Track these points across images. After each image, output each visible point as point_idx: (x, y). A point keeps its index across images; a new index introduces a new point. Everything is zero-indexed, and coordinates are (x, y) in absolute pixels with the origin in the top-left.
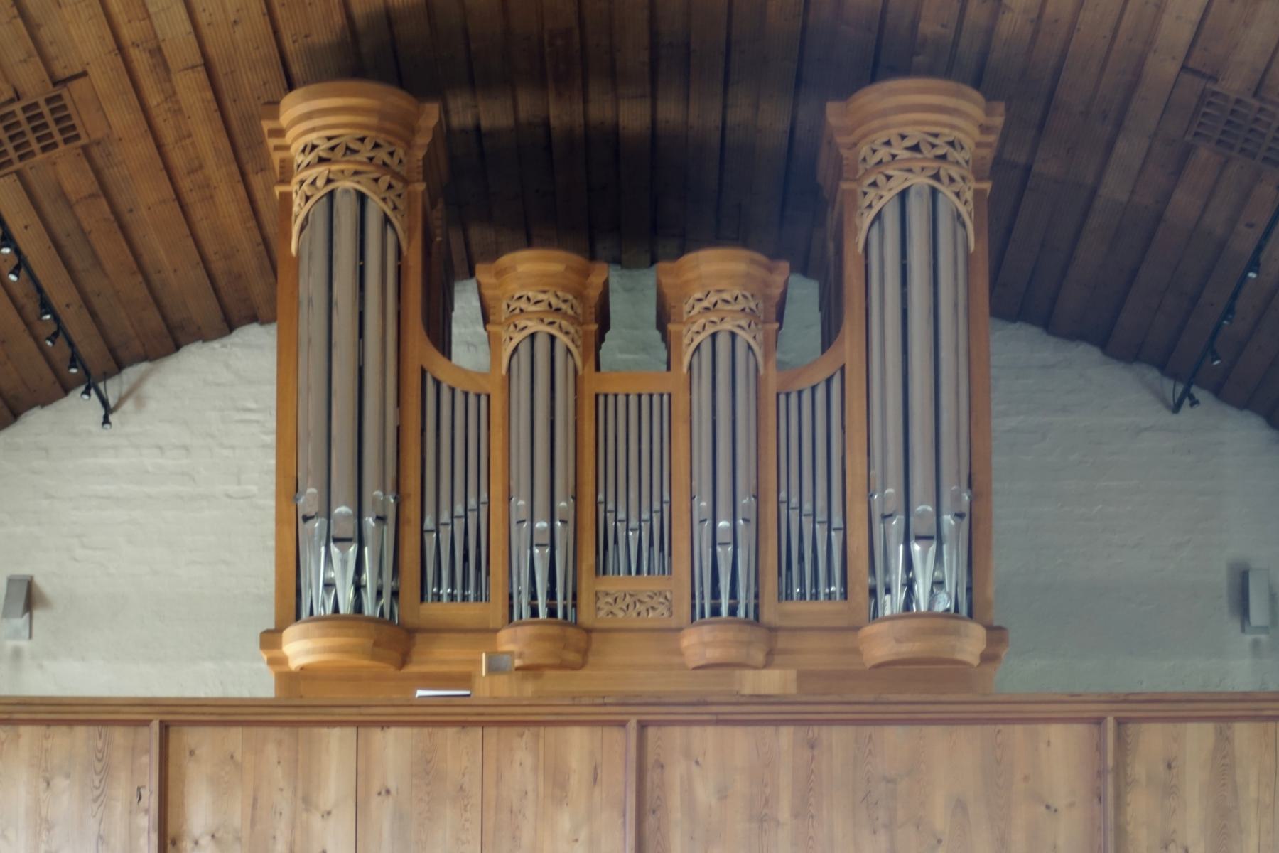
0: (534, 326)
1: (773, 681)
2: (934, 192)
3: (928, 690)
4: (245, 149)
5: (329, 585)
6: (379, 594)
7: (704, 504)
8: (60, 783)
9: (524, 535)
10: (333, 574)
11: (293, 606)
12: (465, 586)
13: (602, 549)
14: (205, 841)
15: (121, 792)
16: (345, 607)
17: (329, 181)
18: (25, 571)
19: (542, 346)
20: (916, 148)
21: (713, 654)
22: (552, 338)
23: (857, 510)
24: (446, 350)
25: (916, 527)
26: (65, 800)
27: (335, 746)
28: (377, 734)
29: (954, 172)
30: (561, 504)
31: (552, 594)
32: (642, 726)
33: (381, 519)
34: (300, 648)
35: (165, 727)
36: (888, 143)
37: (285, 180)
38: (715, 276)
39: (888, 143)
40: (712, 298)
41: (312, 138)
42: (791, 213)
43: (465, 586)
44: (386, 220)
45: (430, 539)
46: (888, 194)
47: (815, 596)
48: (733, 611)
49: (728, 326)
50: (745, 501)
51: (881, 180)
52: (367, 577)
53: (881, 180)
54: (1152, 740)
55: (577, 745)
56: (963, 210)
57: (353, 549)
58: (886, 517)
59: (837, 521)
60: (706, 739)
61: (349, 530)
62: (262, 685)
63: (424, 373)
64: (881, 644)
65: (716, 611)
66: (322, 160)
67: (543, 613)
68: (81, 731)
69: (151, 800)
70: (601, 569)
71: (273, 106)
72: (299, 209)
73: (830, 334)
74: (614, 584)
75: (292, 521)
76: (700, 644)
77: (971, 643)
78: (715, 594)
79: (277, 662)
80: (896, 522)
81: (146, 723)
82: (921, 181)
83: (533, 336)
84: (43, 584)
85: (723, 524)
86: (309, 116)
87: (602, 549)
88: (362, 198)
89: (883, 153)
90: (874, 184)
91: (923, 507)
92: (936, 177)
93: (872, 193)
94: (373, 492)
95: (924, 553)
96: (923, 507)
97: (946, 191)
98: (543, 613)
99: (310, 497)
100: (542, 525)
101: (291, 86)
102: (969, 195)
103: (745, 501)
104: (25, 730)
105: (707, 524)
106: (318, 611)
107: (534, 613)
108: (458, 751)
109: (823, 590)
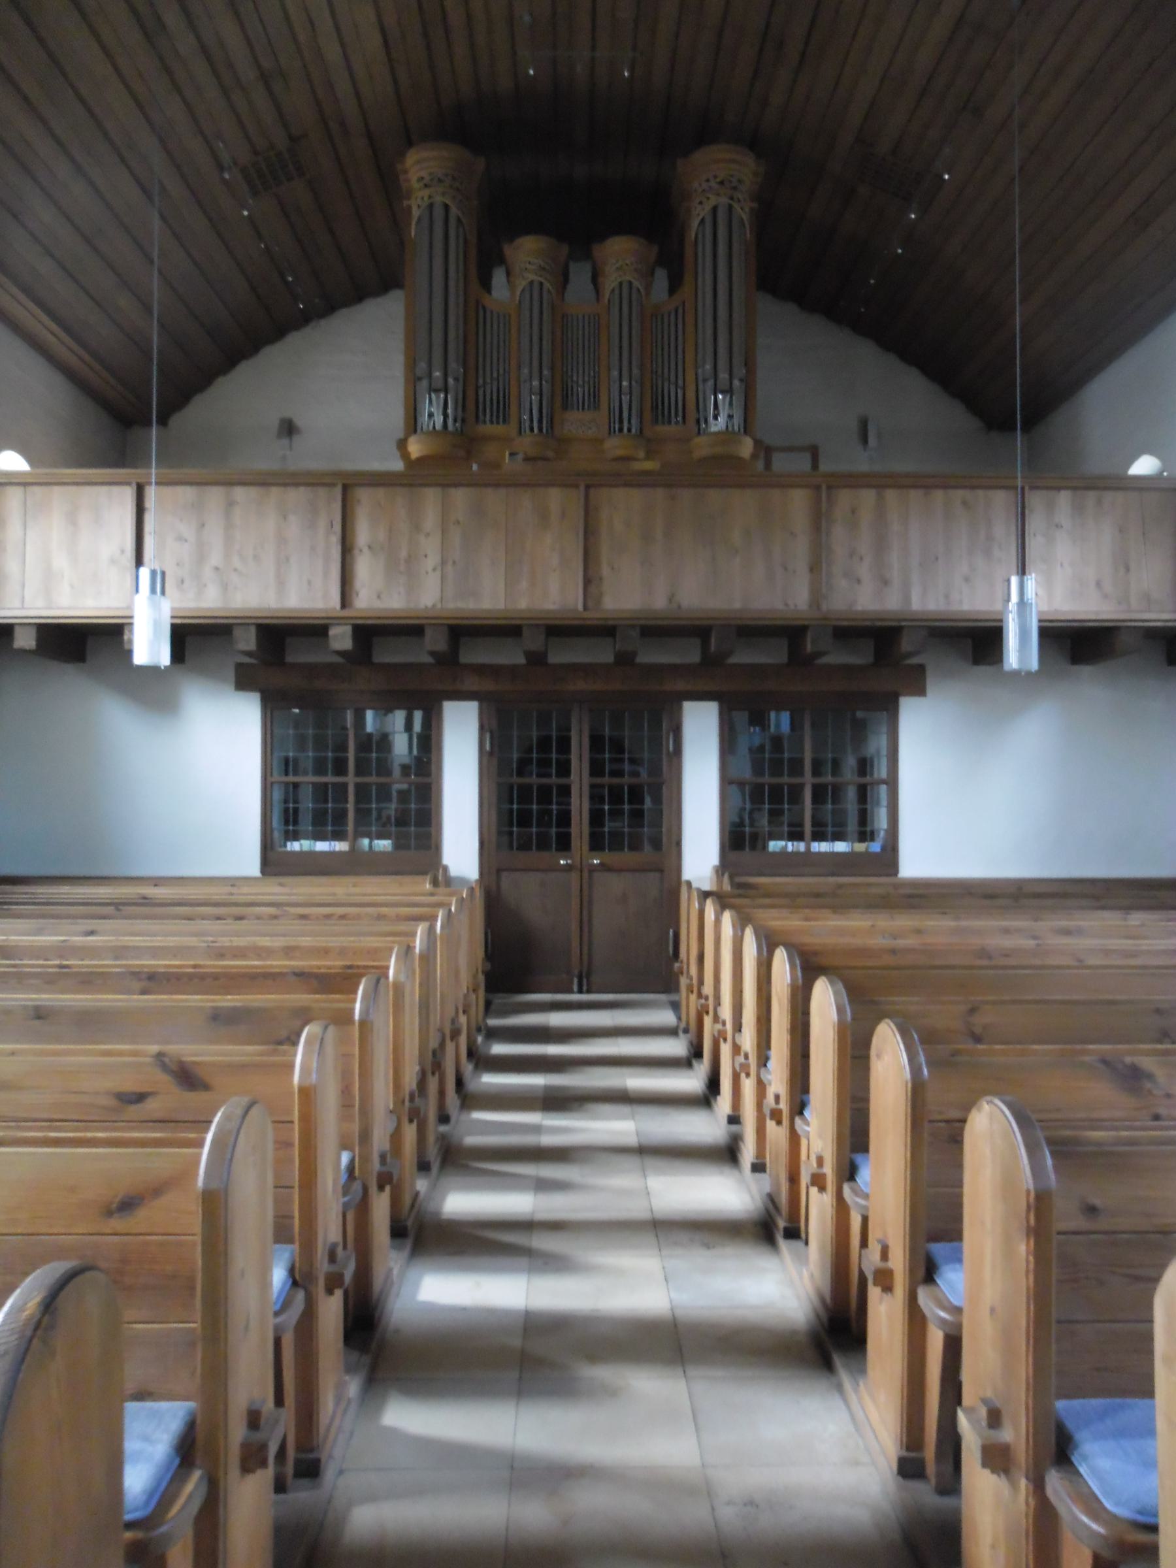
0: (531, 277)
1: (649, 465)
2: (730, 207)
3: (722, 471)
4: (391, 186)
5: (431, 415)
6: (455, 421)
7: (615, 373)
8: (292, 518)
9: (528, 396)
10: (433, 412)
11: (412, 424)
12: (498, 417)
13: (565, 398)
14: (366, 550)
15: (322, 523)
16: (439, 426)
17: (430, 197)
18: (287, 414)
19: (536, 287)
20: (722, 183)
21: (620, 452)
22: (541, 284)
23: (690, 377)
24: (489, 291)
25: (720, 386)
26: (294, 527)
27: (431, 497)
28: (453, 491)
29: (740, 197)
30: (545, 372)
31: (540, 421)
32: (588, 487)
33: (456, 379)
34: (415, 448)
35: (345, 488)
36: (708, 180)
37: (409, 198)
38: (620, 254)
39: (708, 180)
40: (620, 263)
41: (424, 174)
42: (656, 219)
43: (498, 417)
44: (459, 220)
45: (481, 392)
46: (708, 207)
47: (670, 422)
48: (629, 430)
49: (628, 278)
50: (635, 371)
51: (704, 200)
52: (449, 411)
53: (704, 200)
54: (844, 497)
55: (555, 497)
56: (745, 217)
57: (442, 396)
58: (705, 381)
59: (680, 382)
60: (619, 495)
61: (439, 384)
62: (398, 465)
63: (477, 302)
64: (702, 447)
65: (621, 430)
66: (426, 186)
67: (536, 430)
68: (302, 489)
69: (338, 527)
70: (565, 407)
71: (402, 154)
72: (416, 213)
73: (672, 290)
74: (573, 416)
75: (412, 381)
76: (615, 446)
77: (746, 448)
78: (621, 421)
79: (405, 455)
80: (710, 383)
81: (333, 485)
82: (724, 200)
83: (531, 283)
84: (299, 422)
85: (625, 383)
86: (418, 162)
87: (565, 398)
88: (446, 207)
89: (705, 185)
90: (701, 203)
91: (723, 376)
92: (732, 198)
93: (699, 207)
94: (453, 365)
95: (724, 398)
96: (723, 376)
97: (736, 206)
98: (536, 430)
99: (422, 366)
100: (536, 383)
101: (410, 143)
102: (747, 210)
103: (635, 371)
104: (274, 489)
105: (617, 385)
106: (425, 427)
107: (532, 429)
108: (494, 499)
109: (673, 420)
